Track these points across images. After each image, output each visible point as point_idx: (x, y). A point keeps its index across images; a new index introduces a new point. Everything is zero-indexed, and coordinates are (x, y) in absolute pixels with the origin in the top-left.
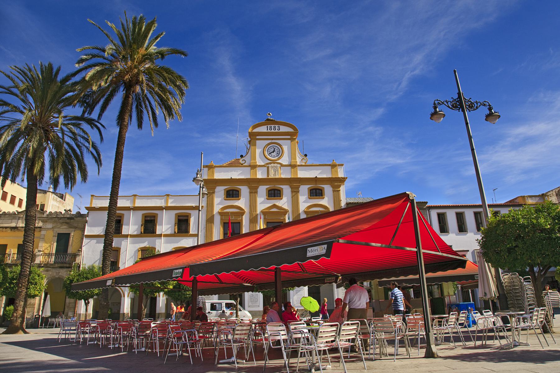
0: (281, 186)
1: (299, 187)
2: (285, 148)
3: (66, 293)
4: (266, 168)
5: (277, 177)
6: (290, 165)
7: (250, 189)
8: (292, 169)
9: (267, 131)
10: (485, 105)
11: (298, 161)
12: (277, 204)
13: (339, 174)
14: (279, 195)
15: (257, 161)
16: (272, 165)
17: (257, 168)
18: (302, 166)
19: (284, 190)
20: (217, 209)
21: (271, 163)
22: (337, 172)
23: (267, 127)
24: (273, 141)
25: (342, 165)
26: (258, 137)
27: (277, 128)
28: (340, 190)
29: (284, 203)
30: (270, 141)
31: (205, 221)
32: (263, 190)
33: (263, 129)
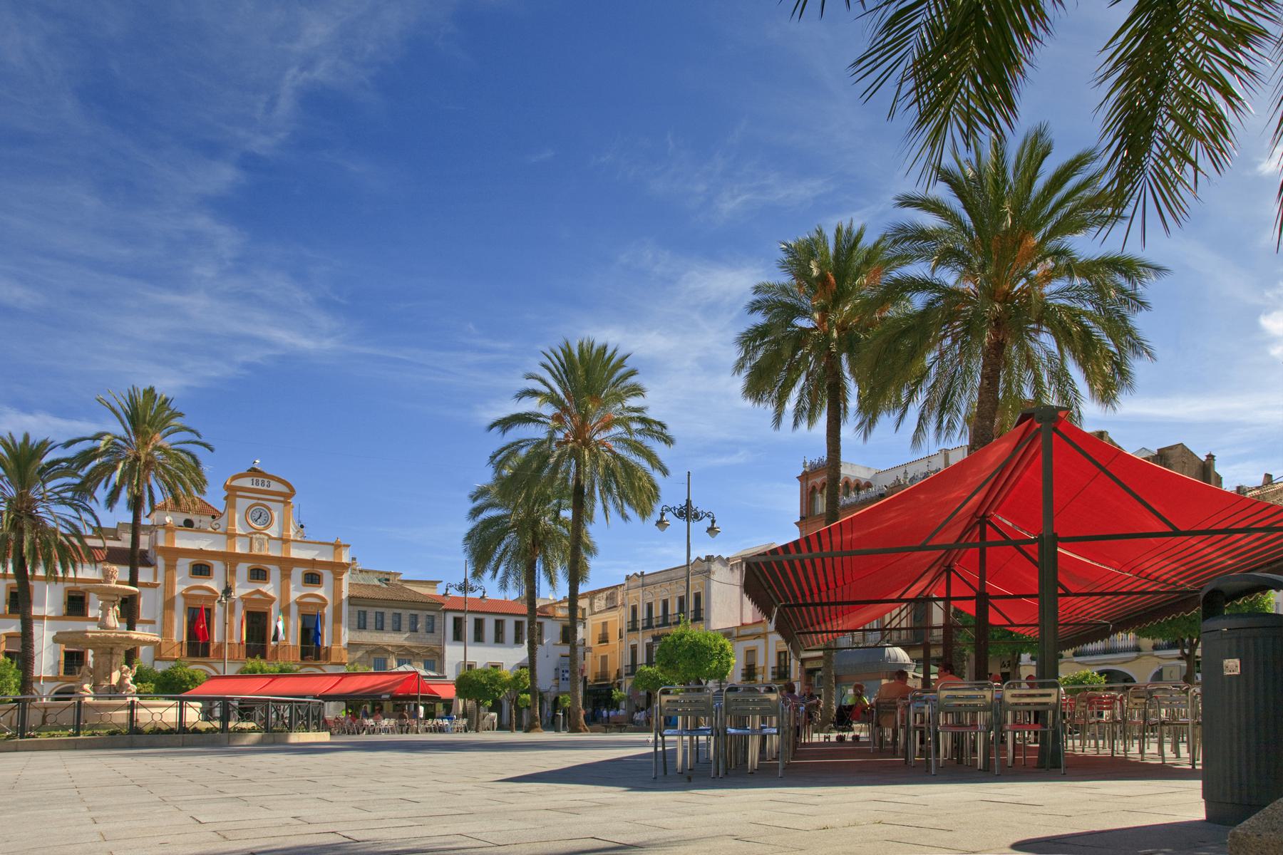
0: (321, 571)
2: (276, 515)
3: (726, 673)
4: (248, 539)
5: (263, 553)
6: (281, 539)
10: (709, 516)
11: (292, 533)
13: (343, 557)
14: (207, 573)
16: (258, 536)
17: (237, 539)
18: (296, 541)
20: (179, 589)
21: (255, 533)
22: (340, 554)
24: (260, 502)
25: (348, 546)
26: (238, 493)
27: (266, 483)
29: (270, 588)
30: (255, 501)
32: (243, 569)
33: (247, 483)
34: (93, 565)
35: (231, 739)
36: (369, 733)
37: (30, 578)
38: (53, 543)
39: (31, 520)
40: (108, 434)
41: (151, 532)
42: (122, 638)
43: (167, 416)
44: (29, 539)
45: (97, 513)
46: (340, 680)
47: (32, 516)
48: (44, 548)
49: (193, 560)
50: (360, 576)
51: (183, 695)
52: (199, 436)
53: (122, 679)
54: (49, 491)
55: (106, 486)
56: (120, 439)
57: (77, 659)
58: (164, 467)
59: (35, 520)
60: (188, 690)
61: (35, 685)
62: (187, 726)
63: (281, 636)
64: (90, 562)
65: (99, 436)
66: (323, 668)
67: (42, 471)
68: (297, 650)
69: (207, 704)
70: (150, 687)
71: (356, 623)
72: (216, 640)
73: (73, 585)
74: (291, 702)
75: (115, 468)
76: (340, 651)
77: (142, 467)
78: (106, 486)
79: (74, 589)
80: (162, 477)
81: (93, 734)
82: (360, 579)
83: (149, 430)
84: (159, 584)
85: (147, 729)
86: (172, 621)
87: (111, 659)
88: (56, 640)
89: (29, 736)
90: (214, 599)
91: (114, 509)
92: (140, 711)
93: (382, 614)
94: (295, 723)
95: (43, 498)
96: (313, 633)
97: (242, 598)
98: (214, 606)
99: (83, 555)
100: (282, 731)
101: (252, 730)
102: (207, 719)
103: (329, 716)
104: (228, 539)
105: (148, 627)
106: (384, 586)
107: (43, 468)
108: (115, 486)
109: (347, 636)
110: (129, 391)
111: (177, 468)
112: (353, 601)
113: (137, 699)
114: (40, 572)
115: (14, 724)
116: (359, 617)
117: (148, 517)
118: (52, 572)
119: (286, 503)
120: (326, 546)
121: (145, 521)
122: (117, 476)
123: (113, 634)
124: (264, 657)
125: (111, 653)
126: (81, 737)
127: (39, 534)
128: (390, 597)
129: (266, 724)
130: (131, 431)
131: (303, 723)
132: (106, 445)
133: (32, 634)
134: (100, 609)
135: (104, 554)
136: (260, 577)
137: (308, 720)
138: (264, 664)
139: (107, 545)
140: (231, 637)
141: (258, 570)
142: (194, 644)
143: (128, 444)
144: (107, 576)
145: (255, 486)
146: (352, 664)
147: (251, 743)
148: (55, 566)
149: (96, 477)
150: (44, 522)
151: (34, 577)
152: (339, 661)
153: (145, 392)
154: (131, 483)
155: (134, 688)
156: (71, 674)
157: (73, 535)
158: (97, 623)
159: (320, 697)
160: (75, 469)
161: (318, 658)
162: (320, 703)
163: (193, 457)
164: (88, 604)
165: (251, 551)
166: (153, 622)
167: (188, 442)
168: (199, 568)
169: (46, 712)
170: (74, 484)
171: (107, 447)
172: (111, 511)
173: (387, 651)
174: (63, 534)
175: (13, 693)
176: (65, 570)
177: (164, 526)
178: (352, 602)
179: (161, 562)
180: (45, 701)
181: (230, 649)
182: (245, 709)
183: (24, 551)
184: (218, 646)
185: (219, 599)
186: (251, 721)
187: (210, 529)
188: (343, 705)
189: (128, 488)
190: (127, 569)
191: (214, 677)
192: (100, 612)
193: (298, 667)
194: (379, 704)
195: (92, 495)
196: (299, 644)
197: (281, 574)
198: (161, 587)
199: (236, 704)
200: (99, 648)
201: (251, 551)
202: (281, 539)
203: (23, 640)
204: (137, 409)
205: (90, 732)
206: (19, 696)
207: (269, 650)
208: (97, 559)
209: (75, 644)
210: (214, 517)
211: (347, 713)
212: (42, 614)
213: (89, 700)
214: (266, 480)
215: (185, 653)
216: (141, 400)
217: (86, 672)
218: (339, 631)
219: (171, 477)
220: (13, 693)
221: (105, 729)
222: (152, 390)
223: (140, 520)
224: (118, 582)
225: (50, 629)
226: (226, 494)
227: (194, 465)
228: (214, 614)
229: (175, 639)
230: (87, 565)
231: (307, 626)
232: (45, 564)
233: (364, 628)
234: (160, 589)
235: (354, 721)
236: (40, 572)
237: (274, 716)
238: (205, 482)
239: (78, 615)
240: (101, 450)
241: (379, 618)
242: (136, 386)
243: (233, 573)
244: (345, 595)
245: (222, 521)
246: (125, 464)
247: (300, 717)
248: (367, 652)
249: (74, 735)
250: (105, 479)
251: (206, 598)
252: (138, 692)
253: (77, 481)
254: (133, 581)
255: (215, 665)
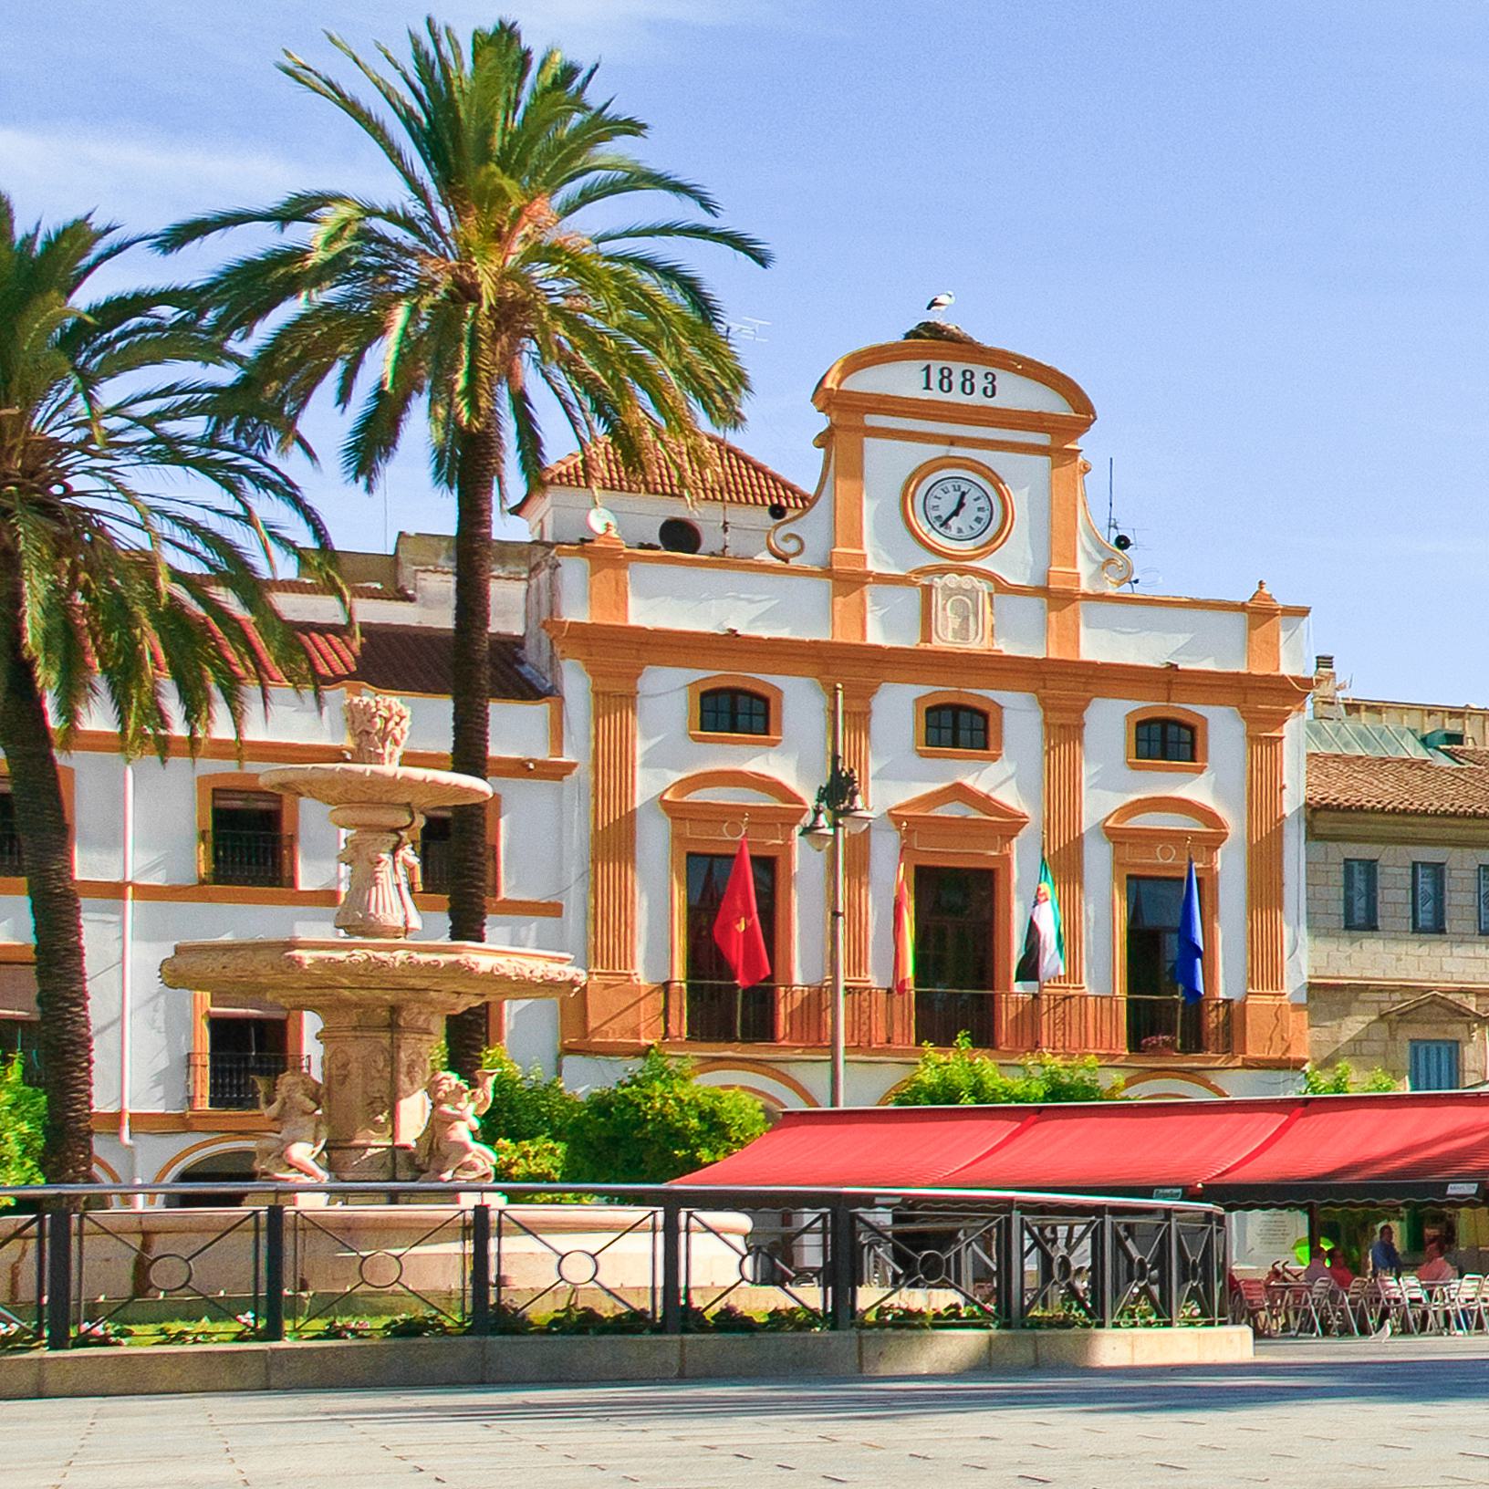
1: (638, 675)
2: (1020, 501)
4: (916, 594)
5: (975, 645)
6: (1043, 591)
7: (593, 674)
8: (1053, 615)
9: (927, 395)
11: (1085, 573)
12: (969, 781)
14: (759, 721)
15: (868, 549)
16: (952, 580)
17: (869, 590)
19: (1006, 713)
20: (648, 785)
21: (942, 571)
22: (1274, 646)
23: (928, 368)
24: (958, 451)
26: (873, 420)
27: (980, 382)
28: (1281, 738)
30: (937, 451)
31: (586, 852)
33: (904, 380)
34: (308, 692)
35: (870, 1352)
36: (1406, 1331)
37: (57, 740)
38: (141, 611)
39: (44, 521)
40: (341, 198)
41: (534, 570)
42: (433, 967)
43: (576, 134)
44: (42, 590)
45: (310, 499)
46: (1284, 1129)
47: (48, 508)
48: (108, 628)
49: (702, 674)
50: (1350, 724)
51: (676, 1186)
52: (706, 204)
53: (438, 1123)
54: (115, 411)
55: (344, 395)
56: (390, 216)
57: (260, 1048)
58: (574, 325)
59: (60, 520)
60: (693, 1165)
61: (99, 1146)
62: (698, 1302)
63: (1051, 961)
64: (296, 681)
65: (300, 209)
66: (1217, 1079)
67: (79, 335)
68: (1114, 1012)
69: (772, 1217)
70: (546, 1155)
71: (1340, 908)
72: (798, 978)
73: (229, 766)
74: (1098, 1210)
75: (376, 329)
76: (1278, 1013)
77: (486, 326)
78: (344, 395)
79: (236, 784)
80: (569, 363)
81: (334, 1333)
82: (1348, 737)
83: (507, 183)
84: (569, 767)
85: (541, 1312)
86: (625, 904)
87: (396, 1046)
88: (176, 974)
89: (84, 1341)
90: (791, 818)
91: (380, 482)
92: (513, 1246)
93: (1438, 870)
94: (1117, 1292)
95: (90, 439)
96: (1172, 945)
97: (895, 817)
98: (787, 848)
99: (268, 657)
100: (1066, 1324)
101: (948, 1320)
102: (772, 1277)
103: (1242, 1267)
104: (1252, 627)
105: (533, 926)
106: (1443, 761)
107: (80, 325)
108: (380, 394)
109: (1304, 957)
110: (416, 44)
111: (626, 328)
112: (1322, 826)
113: (496, 1201)
114: (98, 717)
115: (27, 1292)
116: (1349, 885)
117: (516, 511)
118: (145, 718)
119: (1062, 455)
120: (1208, 614)
121: (505, 528)
122: (380, 361)
123: (401, 955)
124: (984, 1038)
125: (392, 1026)
126: (287, 1343)
127: (84, 576)
128: (1463, 805)
129: (1003, 1295)
130: (432, 189)
131: (1145, 1290)
132: (331, 240)
133: (77, 952)
134: (341, 859)
135: (346, 654)
136: (964, 735)
137: (1164, 1281)
138: (986, 1065)
139: (360, 617)
140: (857, 964)
141: (956, 709)
142: (716, 993)
143: (424, 238)
144: (367, 735)
145: (936, 394)
146: (1327, 1063)
147: (943, 1368)
148: (155, 693)
149: (299, 363)
150: (101, 529)
151: (72, 736)
152: (1274, 1055)
153: (482, 42)
154: (442, 388)
155: (484, 1158)
156: (239, 1104)
157: (222, 579)
158: (333, 911)
159: (1209, 1193)
160: (214, 330)
161: (1194, 1041)
162: (1209, 1216)
163: (690, 287)
164: (293, 838)
166: (553, 909)
167: (667, 230)
168: (725, 703)
169: (146, 1246)
170: (212, 389)
171: (339, 247)
172: (369, 489)
173: (1459, 1012)
174: (177, 576)
175: (14, 1176)
176: (195, 707)
177: (584, 545)
178: (1322, 826)
179: (575, 683)
180: (140, 1203)
181: (855, 1010)
182: (919, 1240)
183: (29, 638)
184: (806, 1001)
185: (808, 819)
186: (942, 1285)
187: (765, 557)
188: (1298, 1223)
189: (433, 402)
190: (442, 709)
191: (793, 1119)
192: (344, 870)
193: (1118, 1077)
194: (1438, 1219)
195: (289, 430)
196: (1121, 991)
197: (1046, 724)
198: (583, 774)
199: (883, 1218)
200: (346, 1005)
202: (1043, 591)
203: (43, 975)
204: (450, 105)
205: (320, 1325)
206: (40, 1186)
207: (1006, 1014)
208: (325, 670)
209: (254, 991)
210: (777, 512)
211: (1316, 1253)
212: (117, 879)
213: (311, 1203)
214: (979, 371)
215: (680, 1025)
216: (465, 68)
217: (299, 1096)
218: (1275, 937)
219: (603, 359)
220: (14, 1176)
221: (377, 1313)
222: (506, 34)
223: (488, 524)
224: (410, 759)
225: (150, 934)
226: (822, 422)
227: (695, 317)
228: (789, 879)
229: (642, 975)
230: (282, 692)
231: (1149, 922)
232: (113, 687)
233: (1370, 925)
235: (1344, 1283)
236: (98, 717)
237: (1032, 1265)
238: (740, 379)
239: (255, 882)
240: (317, 257)
241: (1425, 885)
242: (440, 24)
243: (860, 720)
244: (1292, 802)
245: (812, 528)
246: (414, 311)
247: (1134, 1271)
248: (1382, 1017)
249: (260, 1336)
250: (338, 369)
251: (761, 818)
252: (502, 1173)
253: (226, 375)
254: (469, 754)
255: (797, 1072)
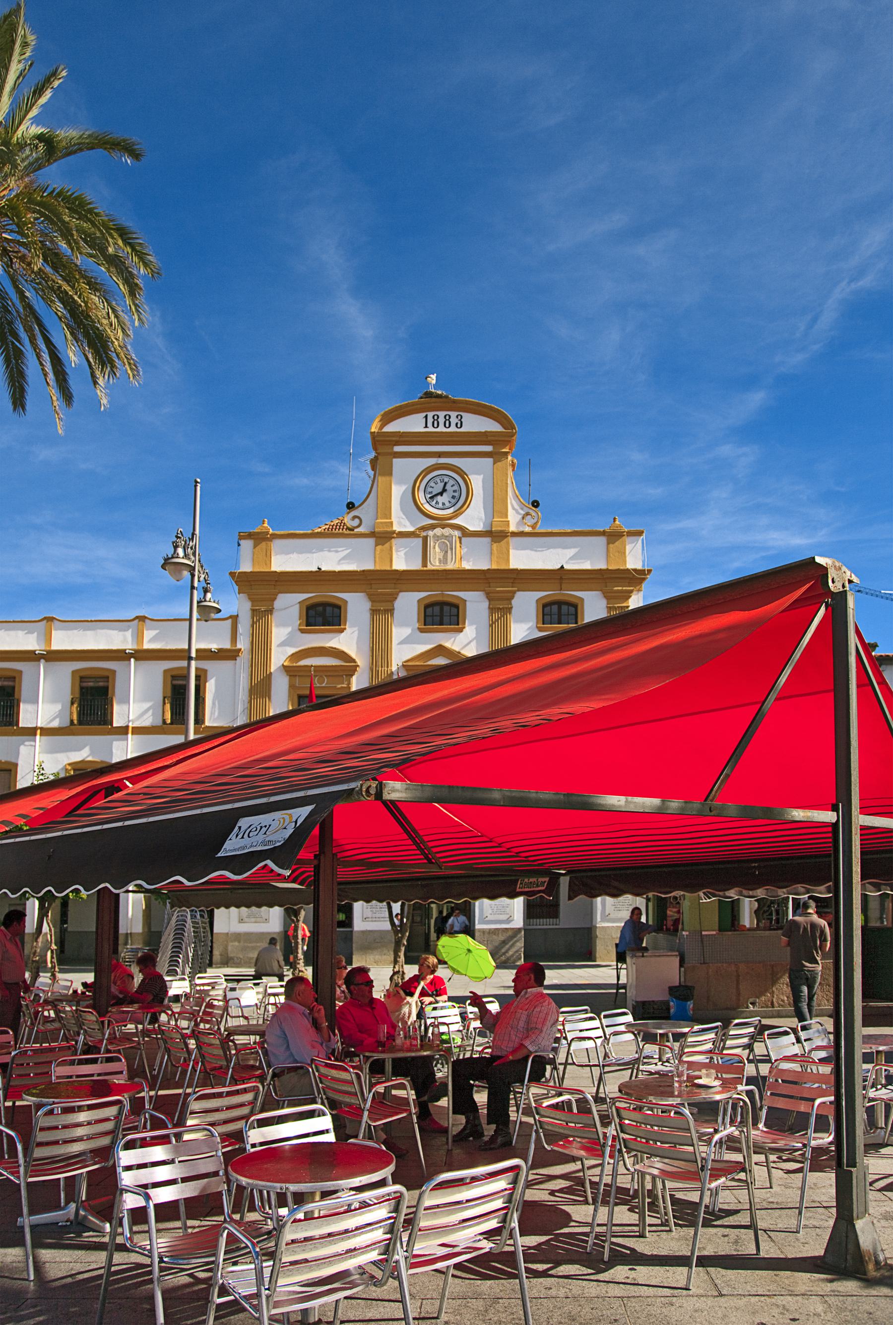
0: (461, 594)
2: (477, 482)
4: (420, 541)
5: (450, 566)
6: (372, 534)
11: (514, 520)
16: (438, 531)
21: (432, 527)
24: (442, 460)
25: (640, 533)
26: (397, 449)
27: (454, 420)
30: (432, 461)
33: (414, 424)
165: (425, 564)
201: (425, 564)
212: (35, 726)
234: (244, 659)
245: (366, 512)
